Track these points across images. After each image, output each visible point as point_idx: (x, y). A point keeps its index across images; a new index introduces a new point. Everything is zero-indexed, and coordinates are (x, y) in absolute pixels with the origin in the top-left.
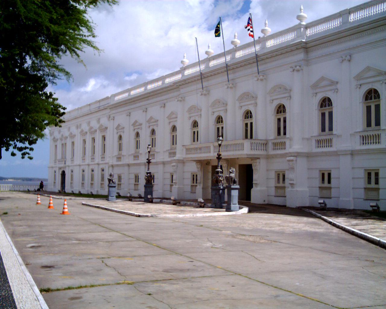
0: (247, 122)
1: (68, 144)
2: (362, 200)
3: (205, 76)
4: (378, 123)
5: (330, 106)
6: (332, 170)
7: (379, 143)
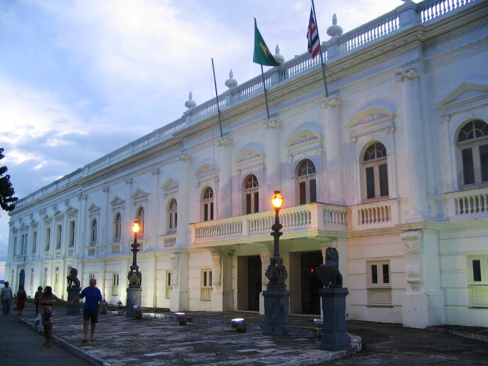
0: (207, 203)
1: (29, 236)
2: (466, 308)
3: (226, 116)
4: (385, 192)
5: (311, 173)
6: (392, 261)
7: (387, 219)
